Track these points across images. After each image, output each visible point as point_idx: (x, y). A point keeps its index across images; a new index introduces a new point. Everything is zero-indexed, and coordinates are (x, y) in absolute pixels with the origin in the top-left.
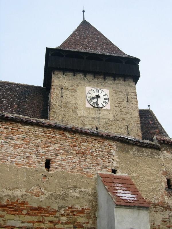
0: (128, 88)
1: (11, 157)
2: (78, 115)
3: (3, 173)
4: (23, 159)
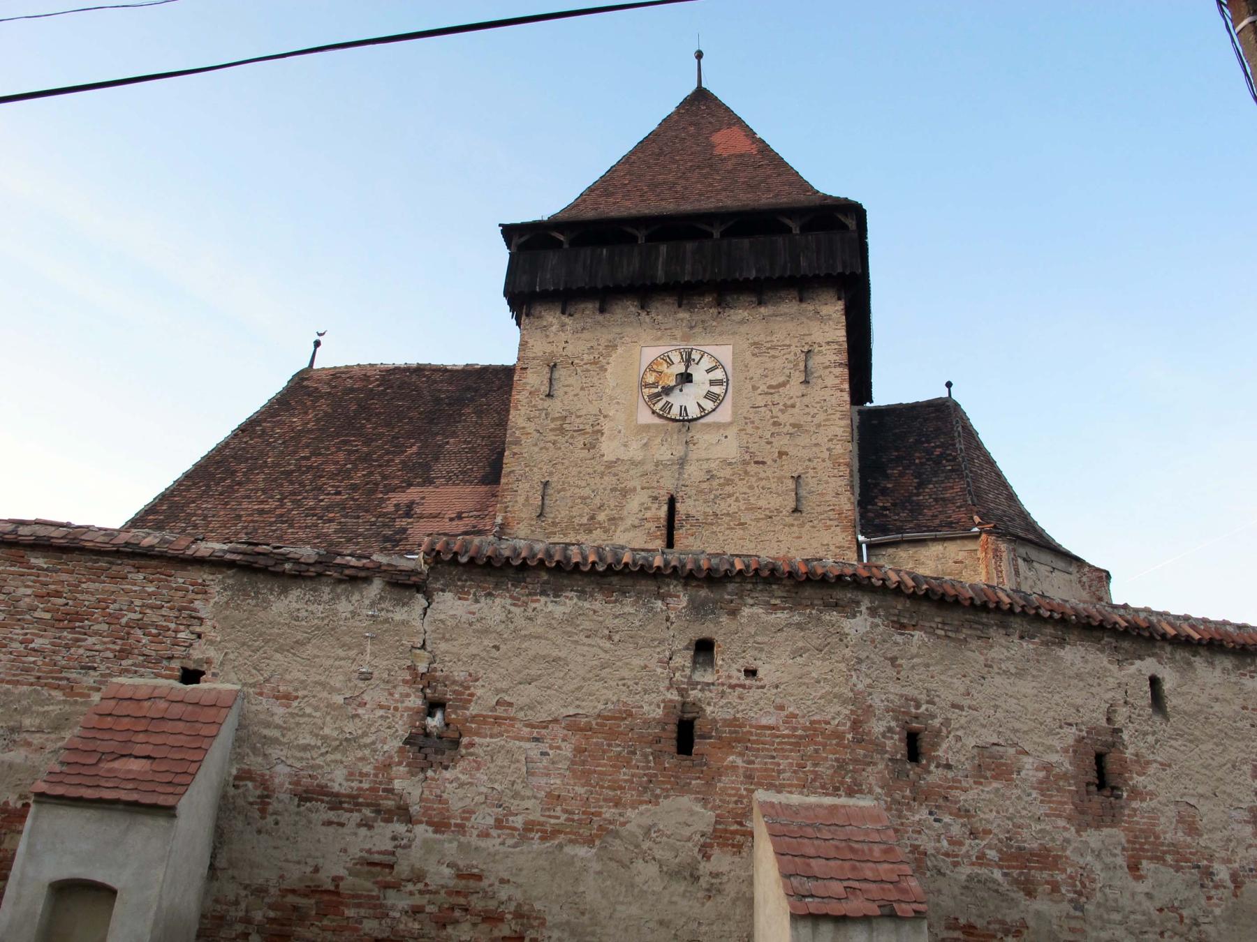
2: (605, 458)
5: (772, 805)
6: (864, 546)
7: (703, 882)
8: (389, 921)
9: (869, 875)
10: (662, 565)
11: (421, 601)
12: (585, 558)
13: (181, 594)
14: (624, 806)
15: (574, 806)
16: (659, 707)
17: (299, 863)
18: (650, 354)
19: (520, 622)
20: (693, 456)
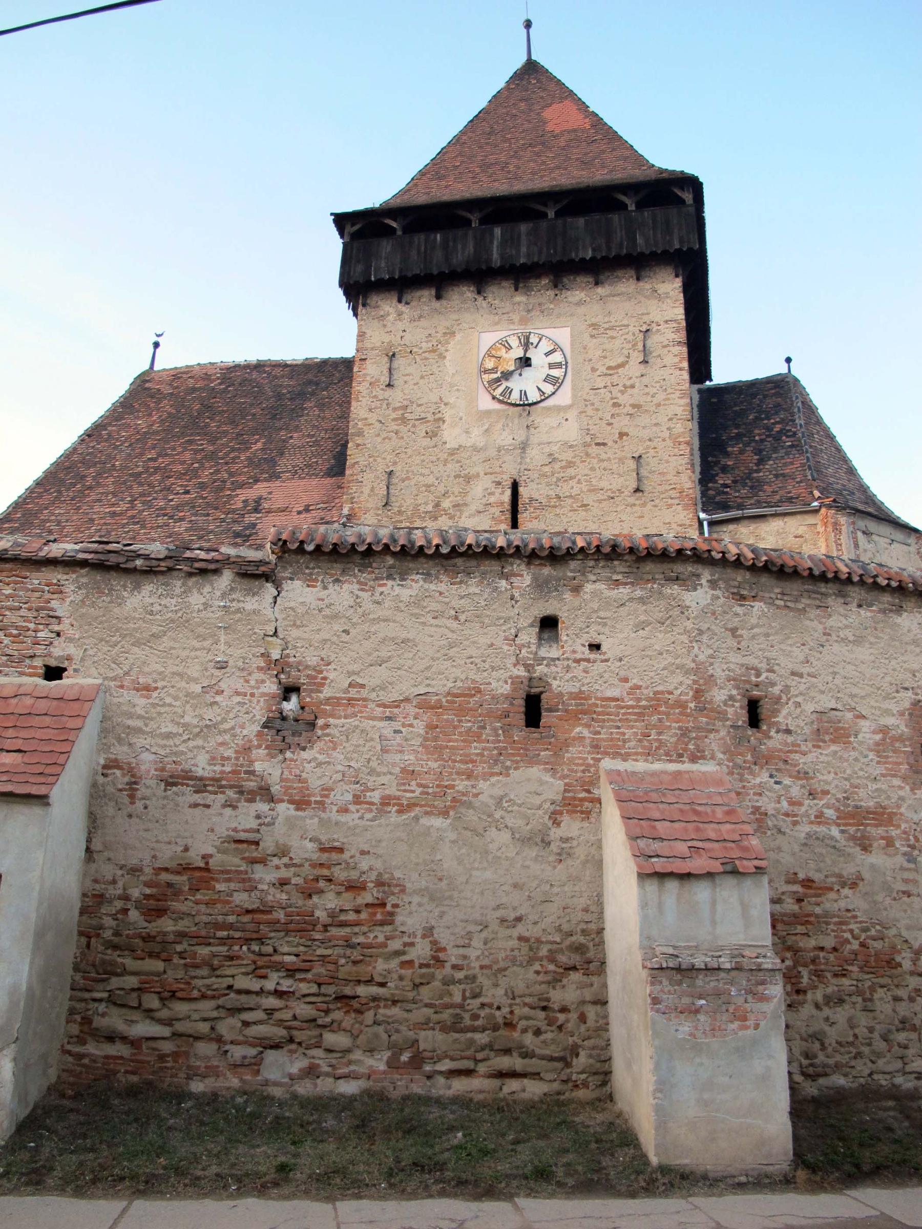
2: (448, 446)
5: (618, 773)
6: (705, 523)
7: (554, 847)
8: (257, 893)
9: (712, 835)
10: (505, 545)
11: (270, 589)
12: (429, 542)
13: (37, 594)
14: (476, 779)
15: (427, 780)
16: (506, 682)
17: (169, 843)
18: (489, 339)
19: (368, 605)
20: (534, 440)
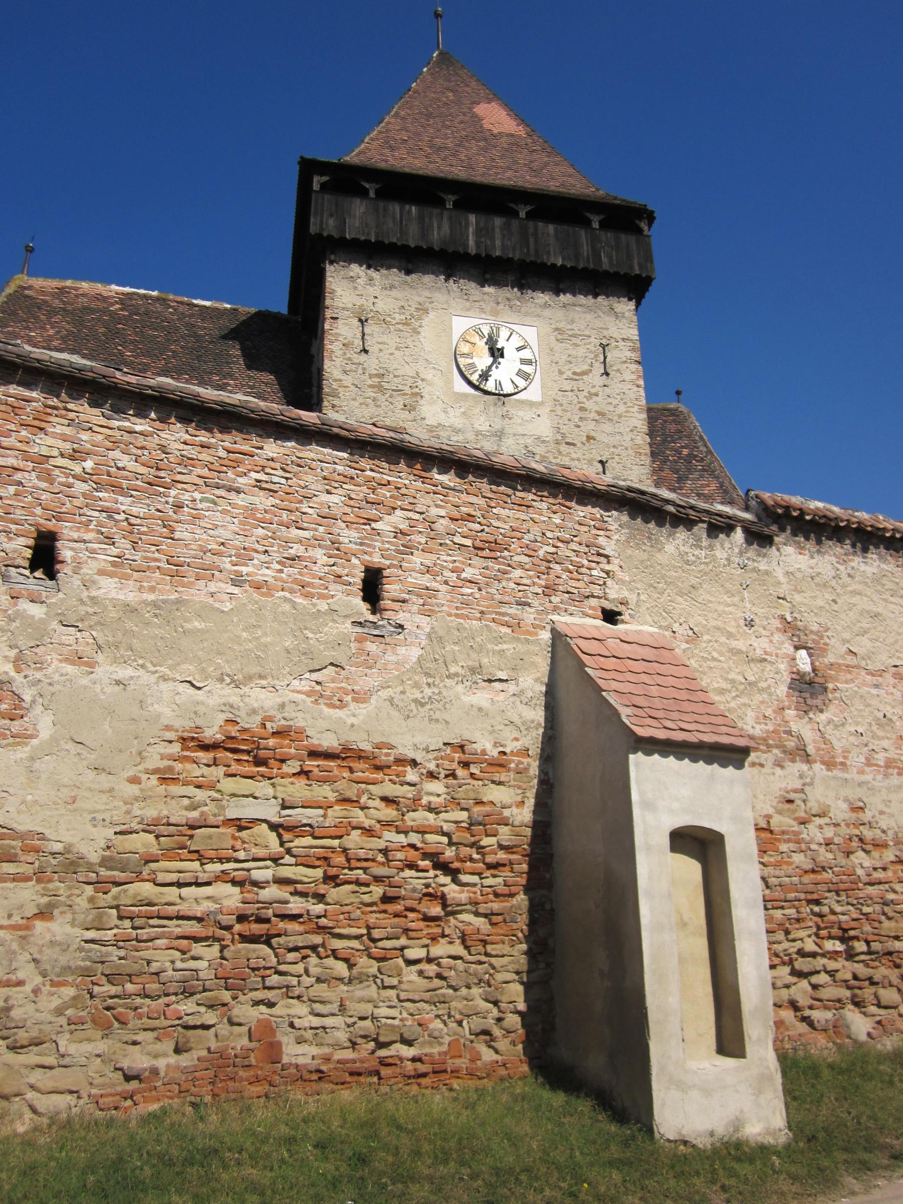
0: (610, 320)
1: (234, 558)
3: (204, 621)
4: (279, 567)
